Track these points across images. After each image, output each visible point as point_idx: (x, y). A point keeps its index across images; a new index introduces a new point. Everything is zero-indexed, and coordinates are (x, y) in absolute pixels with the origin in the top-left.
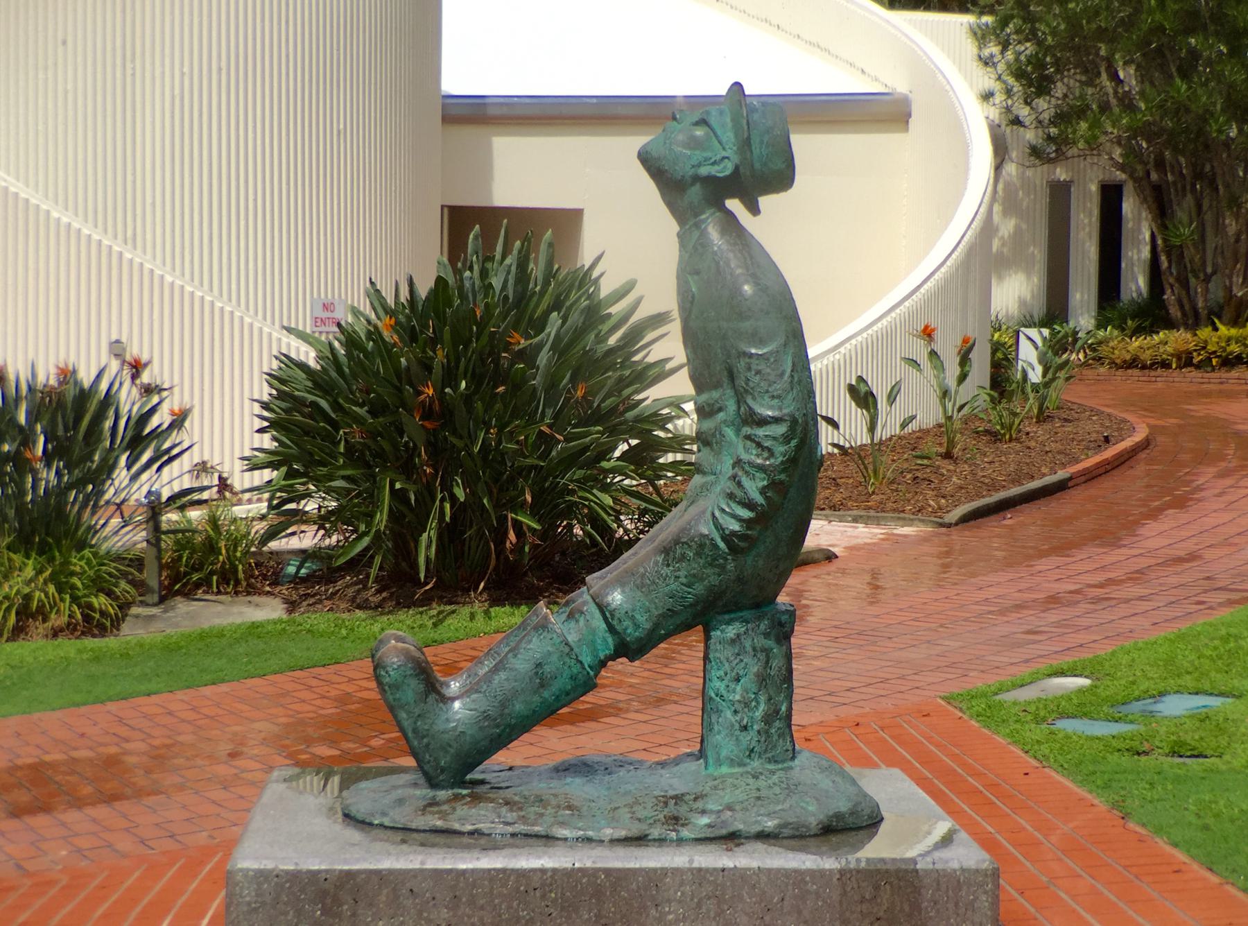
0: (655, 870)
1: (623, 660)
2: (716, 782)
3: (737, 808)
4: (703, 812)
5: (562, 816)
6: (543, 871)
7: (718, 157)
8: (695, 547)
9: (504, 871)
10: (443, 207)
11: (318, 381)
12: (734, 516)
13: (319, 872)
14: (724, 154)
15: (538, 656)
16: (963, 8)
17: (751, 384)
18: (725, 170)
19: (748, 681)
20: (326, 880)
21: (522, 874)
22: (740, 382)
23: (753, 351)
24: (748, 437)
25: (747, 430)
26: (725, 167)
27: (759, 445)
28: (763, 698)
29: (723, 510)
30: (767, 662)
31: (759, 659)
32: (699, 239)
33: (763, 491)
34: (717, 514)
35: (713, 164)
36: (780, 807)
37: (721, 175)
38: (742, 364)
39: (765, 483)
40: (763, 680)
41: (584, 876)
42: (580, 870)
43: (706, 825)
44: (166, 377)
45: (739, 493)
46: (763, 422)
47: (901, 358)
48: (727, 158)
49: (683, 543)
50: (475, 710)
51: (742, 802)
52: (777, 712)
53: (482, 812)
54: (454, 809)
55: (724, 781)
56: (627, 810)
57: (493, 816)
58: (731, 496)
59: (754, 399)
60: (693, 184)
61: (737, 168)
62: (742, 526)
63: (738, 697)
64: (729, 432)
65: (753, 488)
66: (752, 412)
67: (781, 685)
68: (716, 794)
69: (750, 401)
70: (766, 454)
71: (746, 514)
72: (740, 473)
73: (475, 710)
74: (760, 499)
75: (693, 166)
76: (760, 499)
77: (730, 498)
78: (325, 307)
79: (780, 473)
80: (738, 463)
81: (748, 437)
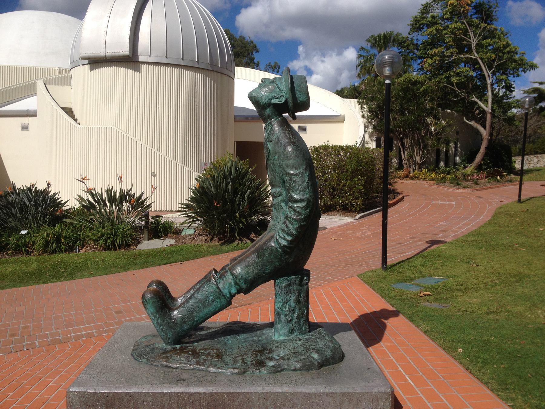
0: (248, 393)
1: (242, 294)
2: (278, 344)
3: (285, 358)
4: (272, 359)
5: (213, 361)
6: (200, 393)
7: (279, 96)
8: (269, 251)
9: (183, 393)
10: (234, 141)
11: (36, 191)
12: (284, 239)
13: (105, 393)
14: (282, 94)
15: (207, 293)
16: (356, 99)
17: (292, 186)
18: (282, 101)
19: (292, 303)
20: (107, 396)
21: (191, 395)
22: (287, 185)
23: (292, 172)
24: (290, 207)
25: (290, 204)
26: (282, 100)
27: (295, 210)
28: (297, 309)
29: (280, 237)
30: (299, 295)
31: (295, 294)
32: (272, 128)
33: (296, 229)
34: (278, 238)
35: (277, 98)
36: (303, 357)
37: (281, 103)
38: (287, 179)
39: (297, 226)
40: (297, 301)
41: (218, 396)
42: (215, 393)
43: (272, 366)
44: (92, 186)
45: (286, 229)
46: (296, 201)
47: (188, 188)
48: (283, 96)
49: (264, 249)
50: (182, 314)
51: (287, 355)
52: (303, 314)
53: (182, 359)
54: (171, 356)
55: (281, 344)
56: (241, 358)
57: (185, 361)
58: (283, 231)
59: (293, 191)
60: (269, 107)
61: (286, 100)
62: (288, 243)
63: (287, 309)
64: (283, 204)
65: (292, 228)
66: (292, 197)
67: (304, 303)
68: (277, 350)
69: (291, 192)
70: (297, 214)
71: (289, 238)
72: (287, 222)
73: (182, 314)
74: (294, 232)
75: (269, 99)
76: (294, 232)
77: (283, 232)
78: (205, 165)
79: (303, 222)
80: (287, 217)
81: (290, 207)
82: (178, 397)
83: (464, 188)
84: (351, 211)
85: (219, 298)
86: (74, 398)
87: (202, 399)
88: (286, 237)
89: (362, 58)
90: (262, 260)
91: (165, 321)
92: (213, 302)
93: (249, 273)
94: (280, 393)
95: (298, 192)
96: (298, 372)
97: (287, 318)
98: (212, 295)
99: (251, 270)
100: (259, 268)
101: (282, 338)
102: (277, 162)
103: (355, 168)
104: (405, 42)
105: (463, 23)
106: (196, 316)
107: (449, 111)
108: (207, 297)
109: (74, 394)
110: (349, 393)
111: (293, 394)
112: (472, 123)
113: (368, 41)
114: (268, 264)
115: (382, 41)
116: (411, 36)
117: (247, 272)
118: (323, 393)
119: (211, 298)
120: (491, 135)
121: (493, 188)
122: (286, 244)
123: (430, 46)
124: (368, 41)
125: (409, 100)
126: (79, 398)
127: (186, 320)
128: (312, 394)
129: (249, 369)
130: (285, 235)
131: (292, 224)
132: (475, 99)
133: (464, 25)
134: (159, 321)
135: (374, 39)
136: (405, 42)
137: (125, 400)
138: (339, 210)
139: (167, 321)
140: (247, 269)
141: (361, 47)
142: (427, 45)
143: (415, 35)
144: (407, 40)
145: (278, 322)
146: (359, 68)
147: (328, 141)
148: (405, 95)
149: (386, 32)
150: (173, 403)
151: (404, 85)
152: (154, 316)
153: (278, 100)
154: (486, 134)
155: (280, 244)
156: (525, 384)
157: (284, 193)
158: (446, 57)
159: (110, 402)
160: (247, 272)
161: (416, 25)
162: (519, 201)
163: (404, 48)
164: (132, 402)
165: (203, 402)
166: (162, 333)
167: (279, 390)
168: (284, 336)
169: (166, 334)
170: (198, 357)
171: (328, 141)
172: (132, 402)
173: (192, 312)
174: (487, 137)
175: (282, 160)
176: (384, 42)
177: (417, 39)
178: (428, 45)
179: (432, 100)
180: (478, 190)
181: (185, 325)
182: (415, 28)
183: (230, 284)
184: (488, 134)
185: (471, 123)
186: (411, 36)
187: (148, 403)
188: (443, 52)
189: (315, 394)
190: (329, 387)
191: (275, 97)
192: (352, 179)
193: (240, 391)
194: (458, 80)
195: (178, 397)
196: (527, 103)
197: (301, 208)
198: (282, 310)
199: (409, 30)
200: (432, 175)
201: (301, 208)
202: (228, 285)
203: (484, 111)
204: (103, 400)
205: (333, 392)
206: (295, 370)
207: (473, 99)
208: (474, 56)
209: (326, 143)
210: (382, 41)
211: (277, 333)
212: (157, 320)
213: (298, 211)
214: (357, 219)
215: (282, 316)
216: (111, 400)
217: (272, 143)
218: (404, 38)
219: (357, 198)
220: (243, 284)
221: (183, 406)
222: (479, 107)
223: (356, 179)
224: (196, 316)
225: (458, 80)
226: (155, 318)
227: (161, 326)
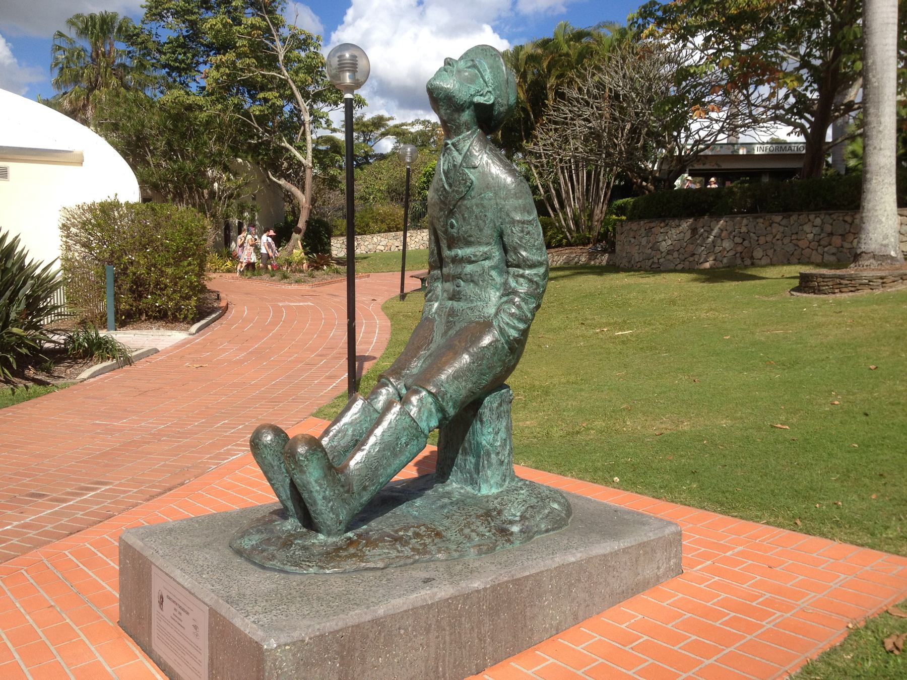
8: (492, 349)
12: (514, 328)
26: (489, 98)
35: (481, 95)
37: (488, 103)
48: (490, 92)
60: (468, 108)
77: (512, 316)
82: (449, 606)
83: (297, 282)
84: (175, 319)
85: (417, 438)
86: (284, 658)
87: (481, 599)
88: (517, 324)
89: (61, 52)
90: (480, 365)
91: (336, 492)
92: (407, 445)
93: (460, 390)
94: (574, 563)
95: (535, 251)
96: (551, 533)
97: (500, 457)
98: (405, 434)
99: (464, 384)
100: (474, 379)
101: (495, 491)
102: (493, 202)
103: (182, 243)
104: (138, 35)
105: (265, 20)
106: (381, 475)
107: (240, 160)
108: (398, 438)
109: (285, 650)
110: (644, 543)
111: (589, 560)
112: (282, 182)
113: (71, 23)
114: (488, 371)
115: (97, 27)
116: (147, 27)
117: (457, 388)
118: (619, 550)
119: (403, 440)
120: (313, 201)
121: (335, 282)
122: (517, 335)
123: (183, 48)
124: (71, 23)
125: (183, 136)
126: (294, 655)
127: (367, 484)
128: (608, 554)
129: (498, 543)
130: (516, 322)
131: (526, 303)
132: (285, 144)
133: (265, 23)
134: (327, 492)
135: (83, 21)
136: (138, 35)
137: (371, 635)
138: (146, 320)
139: (338, 490)
140: (456, 382)
141: (58, 32)
142: (177, 47)
143: (153, 26)
144: (142, 33)
145: (486, 466)
146: (56, 71)
147: (116, 195)
148: (176, 126)
149: (106, 12)
150: (442, 618)
151: (174, 108)
152: (320, 485)
153: (482, 97)
154: (306, 201)
155: (509, 337)
156: (229, 600)
157: (497, 253)
158: (238, 70)
159: (347, 648)
160: (457, 388)
161: (156, 8)
162: (403, 296)
163: (138, 45)
164: (383, 635)
165: (483, 605)
166: (331, 515)
167: (573, 559)
168: (497, 488)
169: (337, 515)
170: (409, 543)
171: (116, 195)
172: (383, 635)
173: (377, 469)
174: (307, 205)
175: (505, 199)
176: (102, 29)
177: (156, 34)
178: (179, 46)
179: (220, 139)
180: (318, 285)
181: (364, 493)
182: (154, 15)
183: (430, 411)
184: (309, 200)
185: (280, 182)
186: (147, 27)
187: (406, 630)
188: (234, 63)
189: (612, 553)
190: (622, 541)
191: (478, 92)
192: (177, 263)
193: (528, 574)
194: (260, 111)
195: (449, 606)
196: (409, 154)
197: (539, 276)
198: (492, 445)
199: (143, 16)
200: (227, 263)
201: (539, 276)
202: (426, 414)
203: (300, 164)
204: (336, 647)
205: (629, 545)
206: (547, 531)
207: (283, 144)
208: (283, 75)
209: (113, 198)
210: (97, 27)
211: (485, 485)
212: (324, 492)
213: (536, 282)
214: (194, 334)
215: (493, 456)
216: (349, 641)
217: (476, 170)
218: (135, 28)
219: (188, 298)
220: (451, 409)
221: (456, 620)
222: (292, 158)
223: (186, 263)
224: (381, 475)
225: (260, 111)
226: (321, 488)
227: (329, 502)
